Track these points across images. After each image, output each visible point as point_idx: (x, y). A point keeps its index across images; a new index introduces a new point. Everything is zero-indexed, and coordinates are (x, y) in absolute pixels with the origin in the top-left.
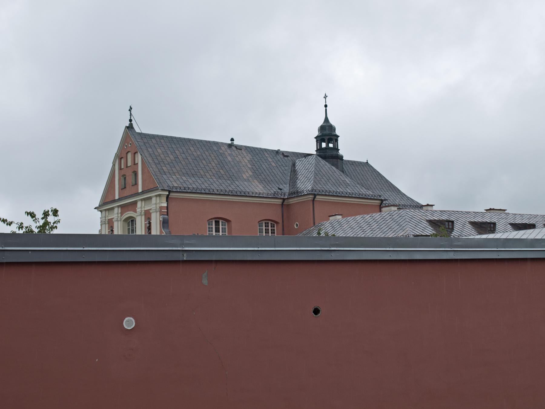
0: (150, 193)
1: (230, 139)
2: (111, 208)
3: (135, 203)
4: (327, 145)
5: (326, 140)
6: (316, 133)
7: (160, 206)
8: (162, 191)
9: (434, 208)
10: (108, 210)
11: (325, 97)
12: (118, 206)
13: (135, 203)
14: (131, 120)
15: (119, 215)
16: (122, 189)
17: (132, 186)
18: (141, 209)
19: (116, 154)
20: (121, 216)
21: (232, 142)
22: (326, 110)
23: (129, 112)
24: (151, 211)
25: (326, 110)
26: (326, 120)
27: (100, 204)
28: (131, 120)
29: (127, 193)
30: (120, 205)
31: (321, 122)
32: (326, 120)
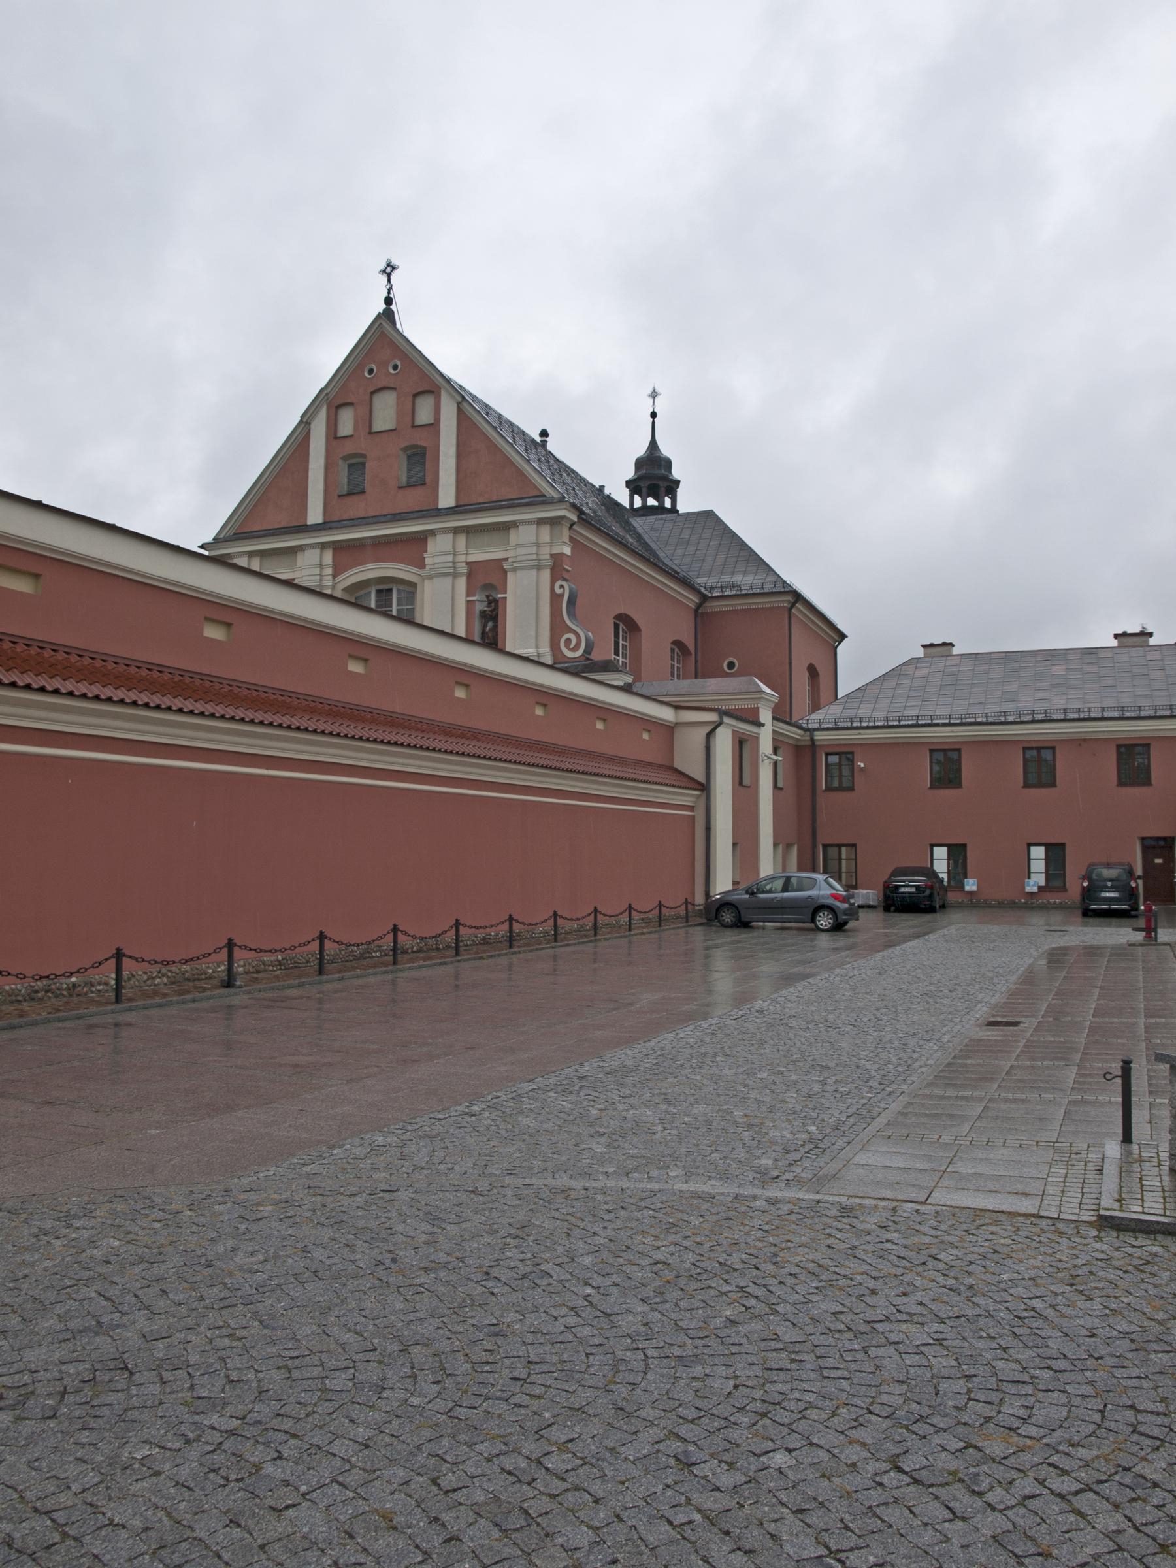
0: (479, 514)
1: (549, 432)
2: (504, 523)
3: (421, 539)
4: (644, 501)
5: (644, 491)
6: (630, 473)
7: (554, 552)
8: (572, 510)
9: (955, 651)
10: (468, 533)
11: (654, 395)
12: (323, 546)
13: (421, 539)
14: (389, 301)
15: (329, 571)
16: (340, 496)
17: (399, 488)
18: (454, 558)
19: (322, 390)
20: (334, 576)
21: (544, 438)
22: (653, 423)
23: (385, 278)
24: (506, 566)
25: (653, 423)
26: (653, 444)
27: (222, 536)
28: (389, 301)
29: (357, 507)
30: (334, 542)
31: (641, 450)
32: (653, 444)
